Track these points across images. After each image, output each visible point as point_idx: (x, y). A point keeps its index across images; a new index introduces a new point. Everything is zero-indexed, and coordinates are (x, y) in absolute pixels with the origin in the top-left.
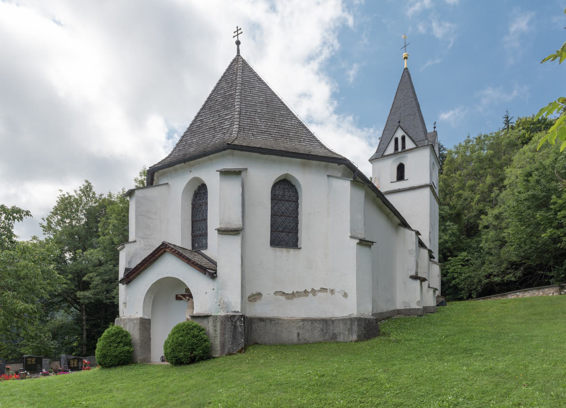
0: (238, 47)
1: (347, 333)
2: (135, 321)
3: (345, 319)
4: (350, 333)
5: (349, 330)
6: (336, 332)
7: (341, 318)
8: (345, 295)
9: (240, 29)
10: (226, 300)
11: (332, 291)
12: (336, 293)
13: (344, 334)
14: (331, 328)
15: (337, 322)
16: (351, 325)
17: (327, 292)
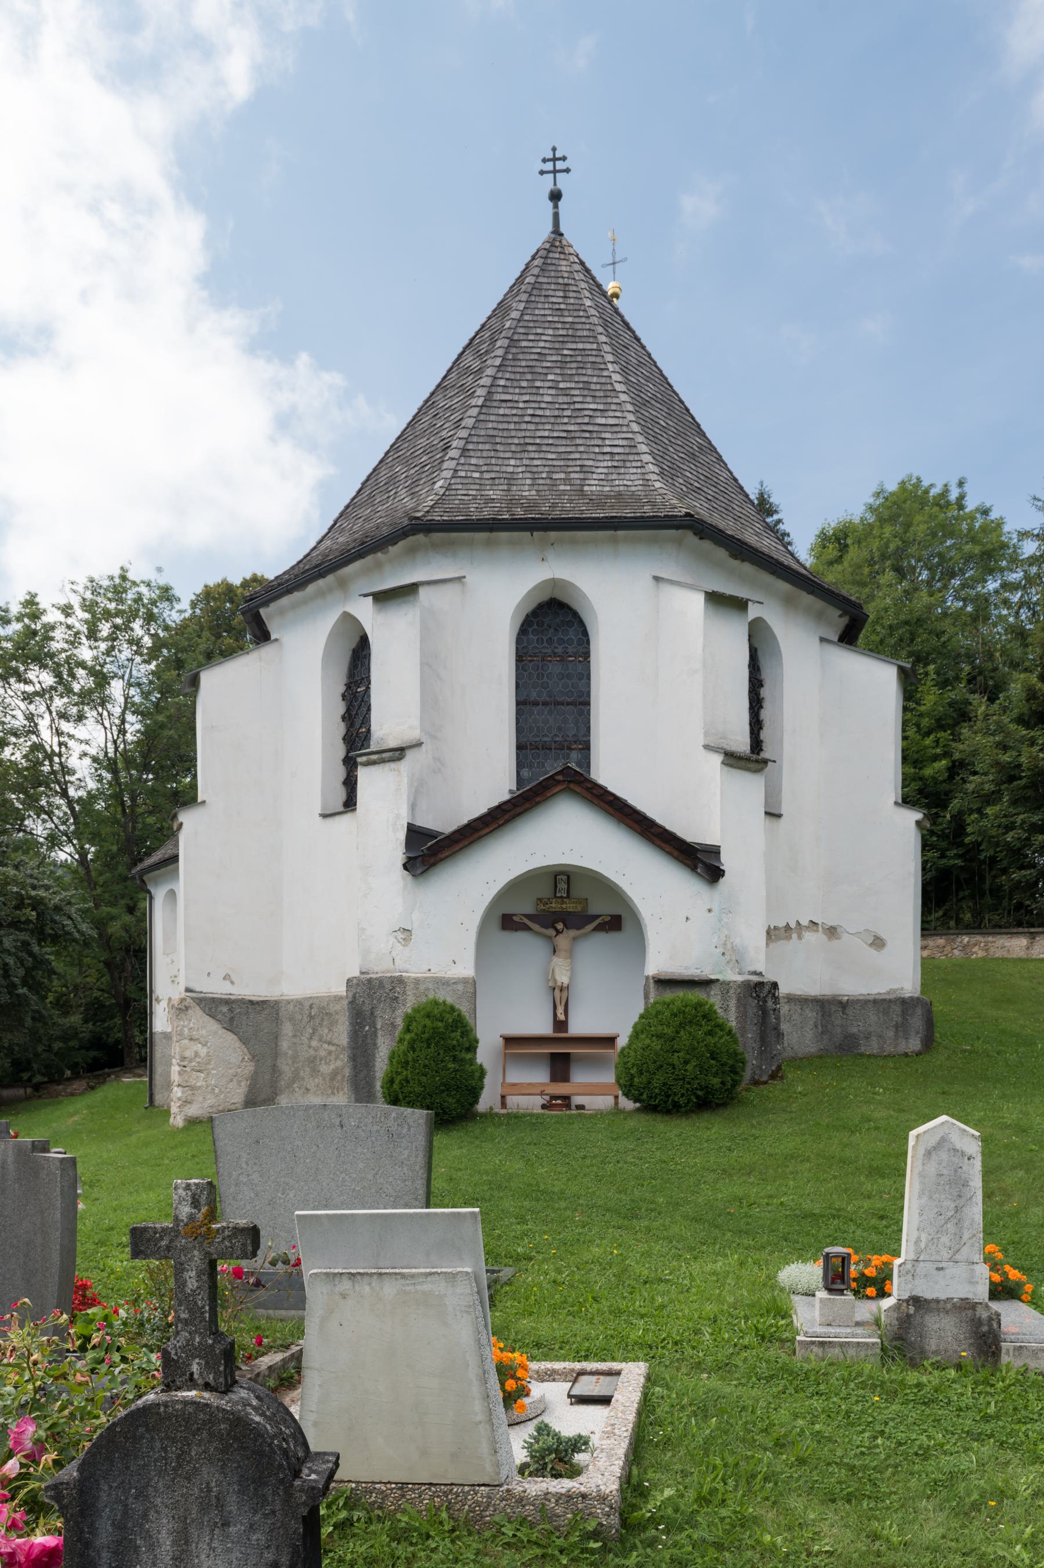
0: (556, 206)
1: (891, 1034)
2: (460, 987)
3: (884, 1000)
4: (901, 1034)
5: (896, 1027)
6: (855, 1030)
7: (871, 998)
8: (878, 943)
9: (564, 159)
10: (737, 941)
11: (832, 932)
12: (845, 937)
13: (880, 1036)
14: (838, 1022)
15: (857, 1007)
16: (904, 1013)
17: (817, 931)
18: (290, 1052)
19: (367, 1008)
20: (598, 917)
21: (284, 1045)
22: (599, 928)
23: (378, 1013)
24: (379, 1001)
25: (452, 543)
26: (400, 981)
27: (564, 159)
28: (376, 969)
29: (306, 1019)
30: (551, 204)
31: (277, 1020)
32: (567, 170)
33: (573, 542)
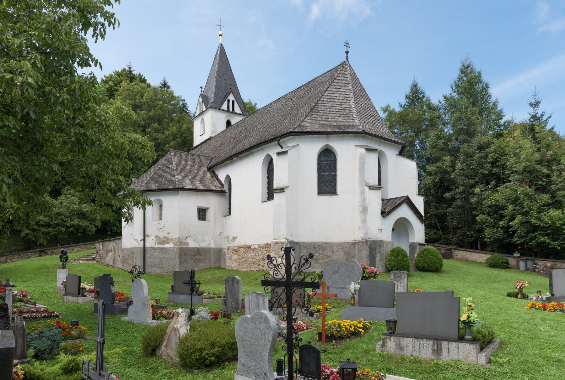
0: (347, 55)
23: (377, 249)
25: (366, 137)
26: (382, 241)
31: (300, 248)
33: (385, 143)
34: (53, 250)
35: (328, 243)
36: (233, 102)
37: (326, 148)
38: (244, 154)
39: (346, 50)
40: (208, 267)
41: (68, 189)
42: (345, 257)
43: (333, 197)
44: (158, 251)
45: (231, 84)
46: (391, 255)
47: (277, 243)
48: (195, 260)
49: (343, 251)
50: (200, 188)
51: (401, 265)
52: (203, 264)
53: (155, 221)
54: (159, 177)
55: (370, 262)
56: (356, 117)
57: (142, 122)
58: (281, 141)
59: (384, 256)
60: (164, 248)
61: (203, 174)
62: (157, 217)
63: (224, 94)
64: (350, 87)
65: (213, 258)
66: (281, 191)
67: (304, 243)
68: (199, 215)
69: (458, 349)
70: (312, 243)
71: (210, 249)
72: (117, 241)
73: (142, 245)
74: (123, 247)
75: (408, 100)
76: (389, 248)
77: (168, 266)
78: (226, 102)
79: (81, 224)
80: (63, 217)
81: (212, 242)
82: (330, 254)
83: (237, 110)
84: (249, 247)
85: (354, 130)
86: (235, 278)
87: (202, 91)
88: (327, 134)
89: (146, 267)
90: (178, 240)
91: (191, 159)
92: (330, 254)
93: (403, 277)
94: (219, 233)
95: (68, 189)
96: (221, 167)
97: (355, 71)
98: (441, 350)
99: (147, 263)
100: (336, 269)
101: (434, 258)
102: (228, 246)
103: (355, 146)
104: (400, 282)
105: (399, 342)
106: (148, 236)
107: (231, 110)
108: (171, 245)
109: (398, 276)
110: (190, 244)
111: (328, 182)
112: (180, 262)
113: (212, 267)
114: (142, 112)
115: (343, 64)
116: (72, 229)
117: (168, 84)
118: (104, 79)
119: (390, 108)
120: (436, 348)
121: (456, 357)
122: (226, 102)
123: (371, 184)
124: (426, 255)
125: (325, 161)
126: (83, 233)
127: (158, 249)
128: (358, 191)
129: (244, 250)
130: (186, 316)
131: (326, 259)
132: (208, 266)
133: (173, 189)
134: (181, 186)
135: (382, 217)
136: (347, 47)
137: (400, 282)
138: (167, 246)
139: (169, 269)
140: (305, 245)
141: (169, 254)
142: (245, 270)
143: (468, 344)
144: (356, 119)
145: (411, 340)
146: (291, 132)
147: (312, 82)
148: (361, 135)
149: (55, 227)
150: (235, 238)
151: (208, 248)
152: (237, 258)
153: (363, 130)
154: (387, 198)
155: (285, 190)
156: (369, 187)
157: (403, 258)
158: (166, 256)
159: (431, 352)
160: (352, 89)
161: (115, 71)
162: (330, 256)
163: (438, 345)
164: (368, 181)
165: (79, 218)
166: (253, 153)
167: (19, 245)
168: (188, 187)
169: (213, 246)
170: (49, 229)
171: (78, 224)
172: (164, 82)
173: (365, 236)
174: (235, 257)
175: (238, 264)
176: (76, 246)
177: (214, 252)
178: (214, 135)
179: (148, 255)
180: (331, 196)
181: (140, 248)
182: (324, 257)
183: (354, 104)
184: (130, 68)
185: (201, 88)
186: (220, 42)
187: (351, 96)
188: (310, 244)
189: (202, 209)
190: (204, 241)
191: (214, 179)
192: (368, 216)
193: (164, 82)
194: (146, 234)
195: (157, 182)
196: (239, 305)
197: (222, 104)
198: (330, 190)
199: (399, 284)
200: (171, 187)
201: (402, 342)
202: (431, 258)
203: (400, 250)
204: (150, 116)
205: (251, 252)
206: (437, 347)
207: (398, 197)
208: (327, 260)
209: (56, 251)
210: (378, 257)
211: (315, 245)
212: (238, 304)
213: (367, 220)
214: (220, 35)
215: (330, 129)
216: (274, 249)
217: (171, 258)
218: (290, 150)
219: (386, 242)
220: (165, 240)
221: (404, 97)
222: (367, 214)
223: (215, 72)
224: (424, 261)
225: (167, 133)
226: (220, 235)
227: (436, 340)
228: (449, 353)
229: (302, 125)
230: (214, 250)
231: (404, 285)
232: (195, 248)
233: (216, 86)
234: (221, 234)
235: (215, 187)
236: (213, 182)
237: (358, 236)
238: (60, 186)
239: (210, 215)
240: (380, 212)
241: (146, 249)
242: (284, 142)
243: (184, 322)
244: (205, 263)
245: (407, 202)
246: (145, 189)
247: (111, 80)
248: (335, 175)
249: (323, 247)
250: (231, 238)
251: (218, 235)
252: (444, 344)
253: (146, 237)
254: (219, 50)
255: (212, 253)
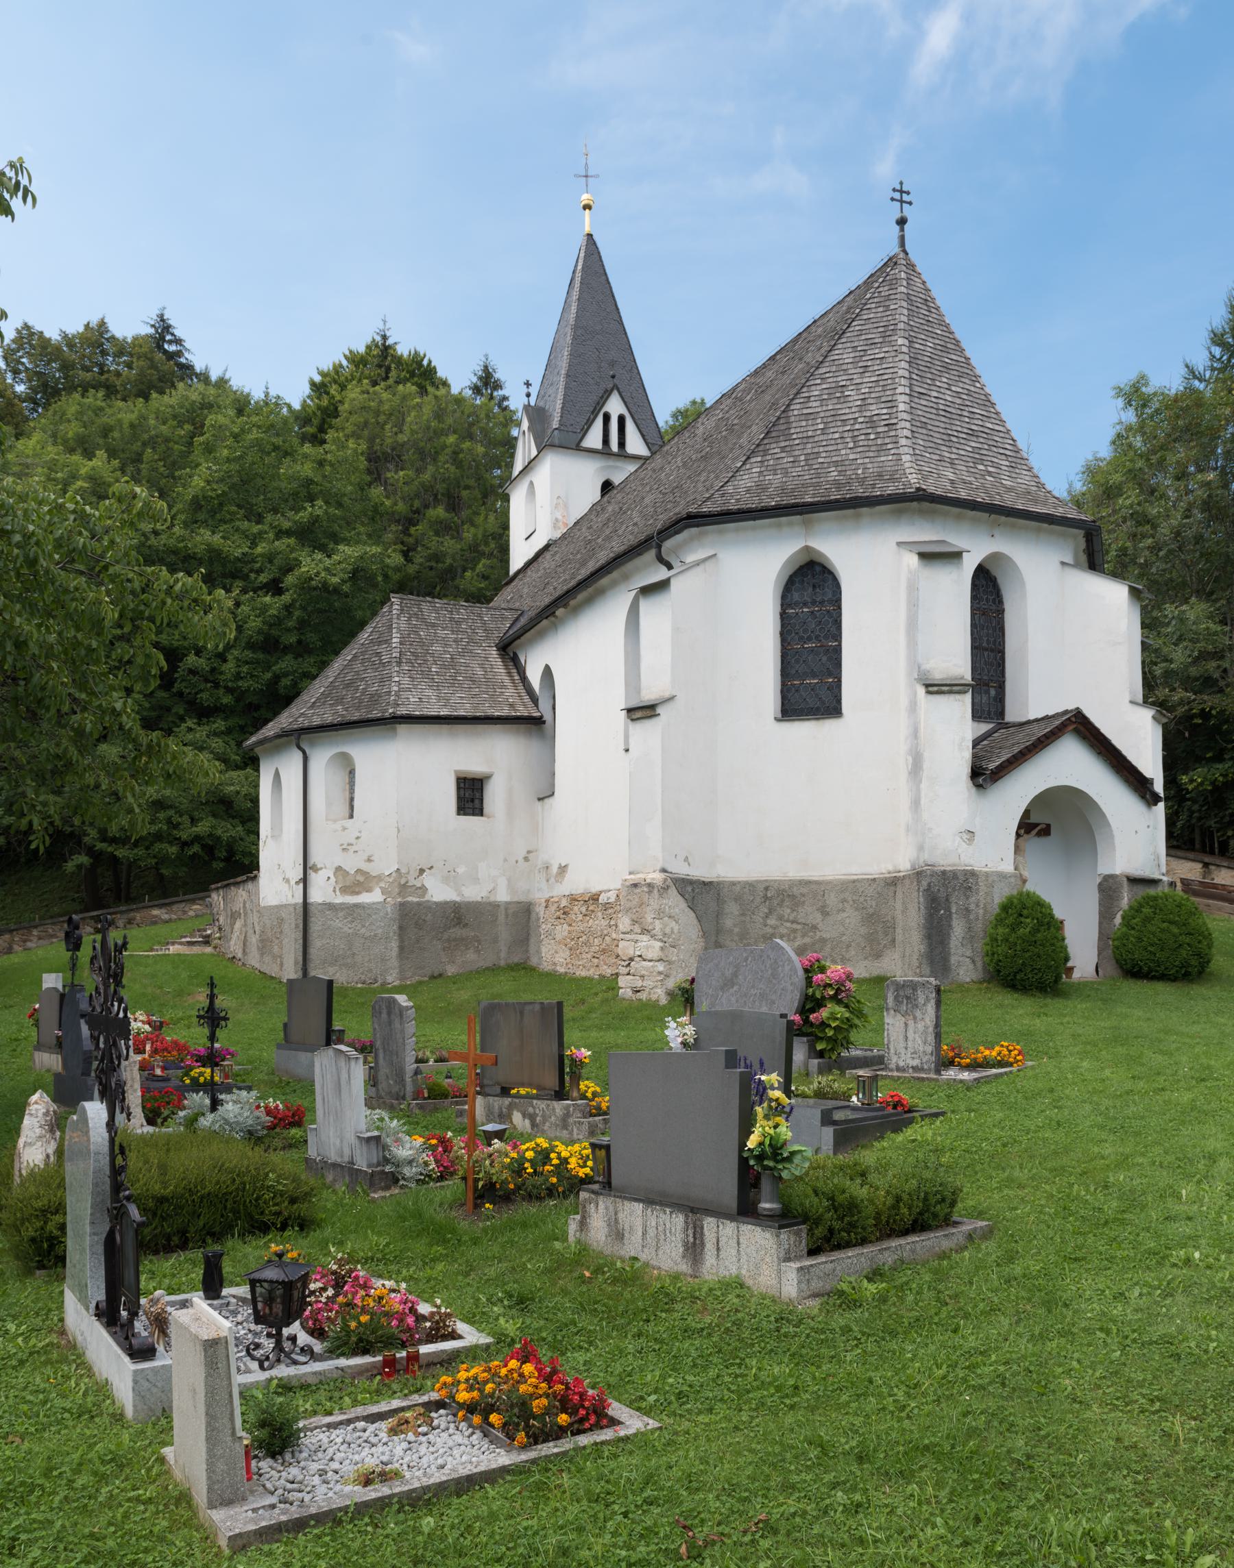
0: (902, 230)
18: (736, 930)
19: (942, 895)
20: (1037, 825)
21: (728, 923)
22: (1039, 834)
23: (953, 899)
24: (954, 889)
25: (934, 512)
26: (973, 874)
27: (908, 193)
28: (942, 863)
29: (758, 900)
30: (898, 228)
31: (719, 900)
32: (910, 203)
33: (1013, 526)
34: (132, 914)
35: (808, 883)
36: (621, 420)
37: (803, 560)
38: (581, 596)
39: (898, 215)
40: (489, 964)
41: (190, 729)
42: (863, 931)
43: (828, 727)
44: (341, 914)
45: (612, 364)
46: (999, 921)
47: (635, 885)
48: (448, 940)
49: (857, 909)
50: (462, 713)
51: (1027, 955)
52: (471, 956)
53: (335, 821)
54: (347, 686)
55: (930, 945)
56: (909, 442)
57: (401, 507)
58: (668, 544)
59: (979, 926)
60: (356, 906)
61: (482, 666)
62: (342, 808)
63: (594, 398)
64: (900, 341)
65: (504, 934)
66: (649, 713)
67: (733, 884)
68: (460, 799)
69: (738, 1243)
70: (758, 882)
71: (496, 906)
72: (250, 885)
73: (299, 899)
74: (262, 904)
75: (1217, 351)
76: (1000, 895)
77: (370, 961)
78: (599, 423)
79: (219, 832)
80: (171, 812)
81: (502, 883)
82: (817, 918)
83: (635, 444)
84: (595, 898)
85: (891, 489)
86: (395, 1000)
87: (528, 395)
88: (801, 514)
89: (311, 966)
90: (395, 880)
91: (452, 619)
92: (817, 918)
93: (921, 1000)
94: (524, 853)
95: (190, 729)
96: (532, 642)
97: (929, 285)
98: (703, 1244)
99: (313, 951)
100: (728, 973)
101: (1176, 930)
102: (547, 896)
103: (899, 544)
104: (915, 1018)
105: (616, 1214)
106: (316, 869)
107: (614, 446)
108: (373, 897)
109: (908, 998)
110: (430, 892)
111: (814, 676)
112: (401, 948)
113: (502, 963)
114: (401, 473)
115: (892, 262)
116: (196, 848)
117: (497, 376)
118: (318, 379)
119: (1146, 385)
120: (691, 1240)
121: (734, 1271)
122: (599, 423)
123: (938, 676)
124: (1147, 920)
125: (805, 604)
126: (227, 860)
127: (342, 909)
128: (904, 702)
129: (584, 909)
130: (46, 1114)
131: (803, 936)
132: (487, 960)
133: (378, 720)
134: (402, 711)
135: (974, 789)
136: (902, 202)
137: (915, 1018)
138: (365, 898)
139: (370, 971)
140: (738, 888)
141: (371, 924)
142: (584, 973)
143: (759, 1229)
144: (906, 450)
145: (638, 1207)
146: (690, 517)
147: (804, 335)
148: (915, 504)
149: (152, 844)
150: (563, 869)
151: (490, 904)
152: (566, 933)
153: (918, 489)
154: (1024, 720)
155: (659, 710)
156: (927, 686)
157: (1035, 931)
158: (363, 931)
159: (681, 1250)
160: (905, 349)
161: (347, 353)
162: (814, 928)
163: (695, 1228)
164: (926, 666)
165: (214, 816)
166: (601, 592)
167: (73, 900)
168: (426, 712)
169: (503, 896)
170: (136, 851)
171: (211, 835)
172: (486, 368)
173: (918, 858)
174: (562, 931)
175: (568, 953)
176: (193, 901)
177: (507, 916)
178: (558, 535)
179: (316, 926)
180: (821, 722)
181: (295, 905)
182: (795, 931)
183: (906, 399)
184: (385, 338)
185: (528, 384)
186: (587, 229)
187: (901, 373)
188: (751, 886)
189: (473, 779)
190: (476, 880)
191: (513, 681)
192: (923, 786)
193: (486, 368)
194: (310, 864)
195: (340, 701)
196: (404, 1086)
197: (585, 432)
198: (823, 703)
199: (911, 1023)
200: (376, 714)
201: (621, 1216)
202: (1163, 931)
203: (1029, 904)
204: (422, 484)
205: (600, 914)
206: (695, 1238)
207: (1050, 713)
208: (807, 940)
209: (138, 916)
210: (958, 929)
211: (767, 889)
212: (402, 1081)
213: (922, 802)
214: (587, 207)
215: (814, 495)
216: (629, 905)
217: (375, 935)
218: (681, 578)
219: (987, 874)
220: (361, 879)
221: (1204, 337)
222: (920, 781)
223: (569, 331)
224: (1140, 939)
225: (468, 534)
226: (526, 859)
227: (693, 1210)
228: (718, 1256)
229: (729, 488)
230: (506, 909)
231: (926, 1027)
232: (446, 903)
233: (568, 375)
234: (531, 856)
235: (512, 706)
236: (510, 692)
237: (902, 860)
238: (170, 719)
239: (494, 796)
240: (966, 770)
241: (312, 909)
242: (675, 551)
243: (38, 1131)
244: (478, 951)
245: (1077, 732)
246: (306, 724)
247: (335, 382)
248: (838, 650)
249: (793, 897)
250: (555, 869)
251: (521, 860)
252: (709, 1223)
253: (309, 871)
254: (582, 255)
255: (501, 918)
